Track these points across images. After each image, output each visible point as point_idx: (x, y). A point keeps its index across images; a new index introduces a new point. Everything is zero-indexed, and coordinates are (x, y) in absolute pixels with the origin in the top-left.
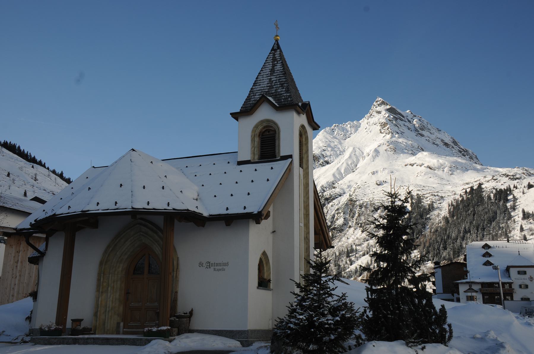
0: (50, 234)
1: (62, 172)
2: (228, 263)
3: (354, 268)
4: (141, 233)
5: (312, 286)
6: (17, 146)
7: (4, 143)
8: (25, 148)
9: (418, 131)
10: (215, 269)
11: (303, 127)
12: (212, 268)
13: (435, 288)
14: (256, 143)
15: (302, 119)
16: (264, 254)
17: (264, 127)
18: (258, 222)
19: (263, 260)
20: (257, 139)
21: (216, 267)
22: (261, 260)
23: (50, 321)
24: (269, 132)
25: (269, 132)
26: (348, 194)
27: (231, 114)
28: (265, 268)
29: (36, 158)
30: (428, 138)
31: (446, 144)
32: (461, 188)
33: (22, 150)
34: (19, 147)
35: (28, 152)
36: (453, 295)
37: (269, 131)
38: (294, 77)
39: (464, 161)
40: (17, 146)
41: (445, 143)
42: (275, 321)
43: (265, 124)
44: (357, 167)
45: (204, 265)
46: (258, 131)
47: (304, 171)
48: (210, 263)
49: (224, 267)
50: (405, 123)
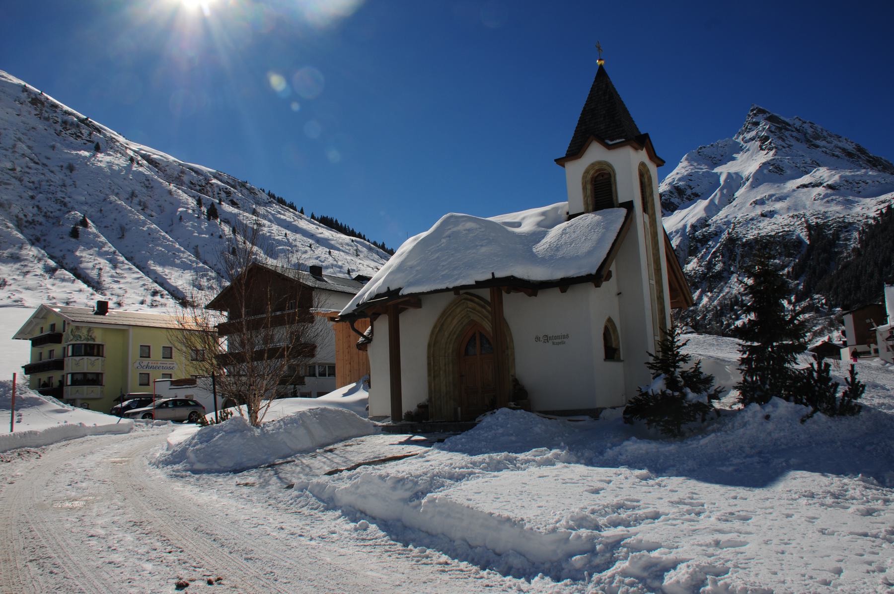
0: (374, 317)
2: (567, 335)
3: (741, 324)
4: (468, 309)
6: (334, 220)
7: (321, 218)
8: (342, 221)
9: (811, 141)
10: (553, 343)
11: (643, 164)
12: (550, 342)
13: (845, 340)
14: (589, 192)
15: (642, 156)
16: (610, 320)
17: (597, 171)
18: (598, 285)
19: (610, 327)
20: (589, 187)
21: (554, 341)
22: (606, 329)
24: (603, 176)
25: (603, 176)
26: (726, 232)
27: (556, 160)
28: (613, 337)
29: (355, 230)
30: (824, 149)
31: (849, 154)
32: (875, 209)
34: (336, 221)
36: (869, 346)
37: (602, 175)
38: (627, 106)
39: (875, 174)
40: (334, 220)
41: (848, 152)
43: (596, 168)
44: (735, 197)
45: (541, 339)
46: (589, 177)
47: (649, 218)
48: (547, 336)
49: (564, 340)
50: (792, 133)
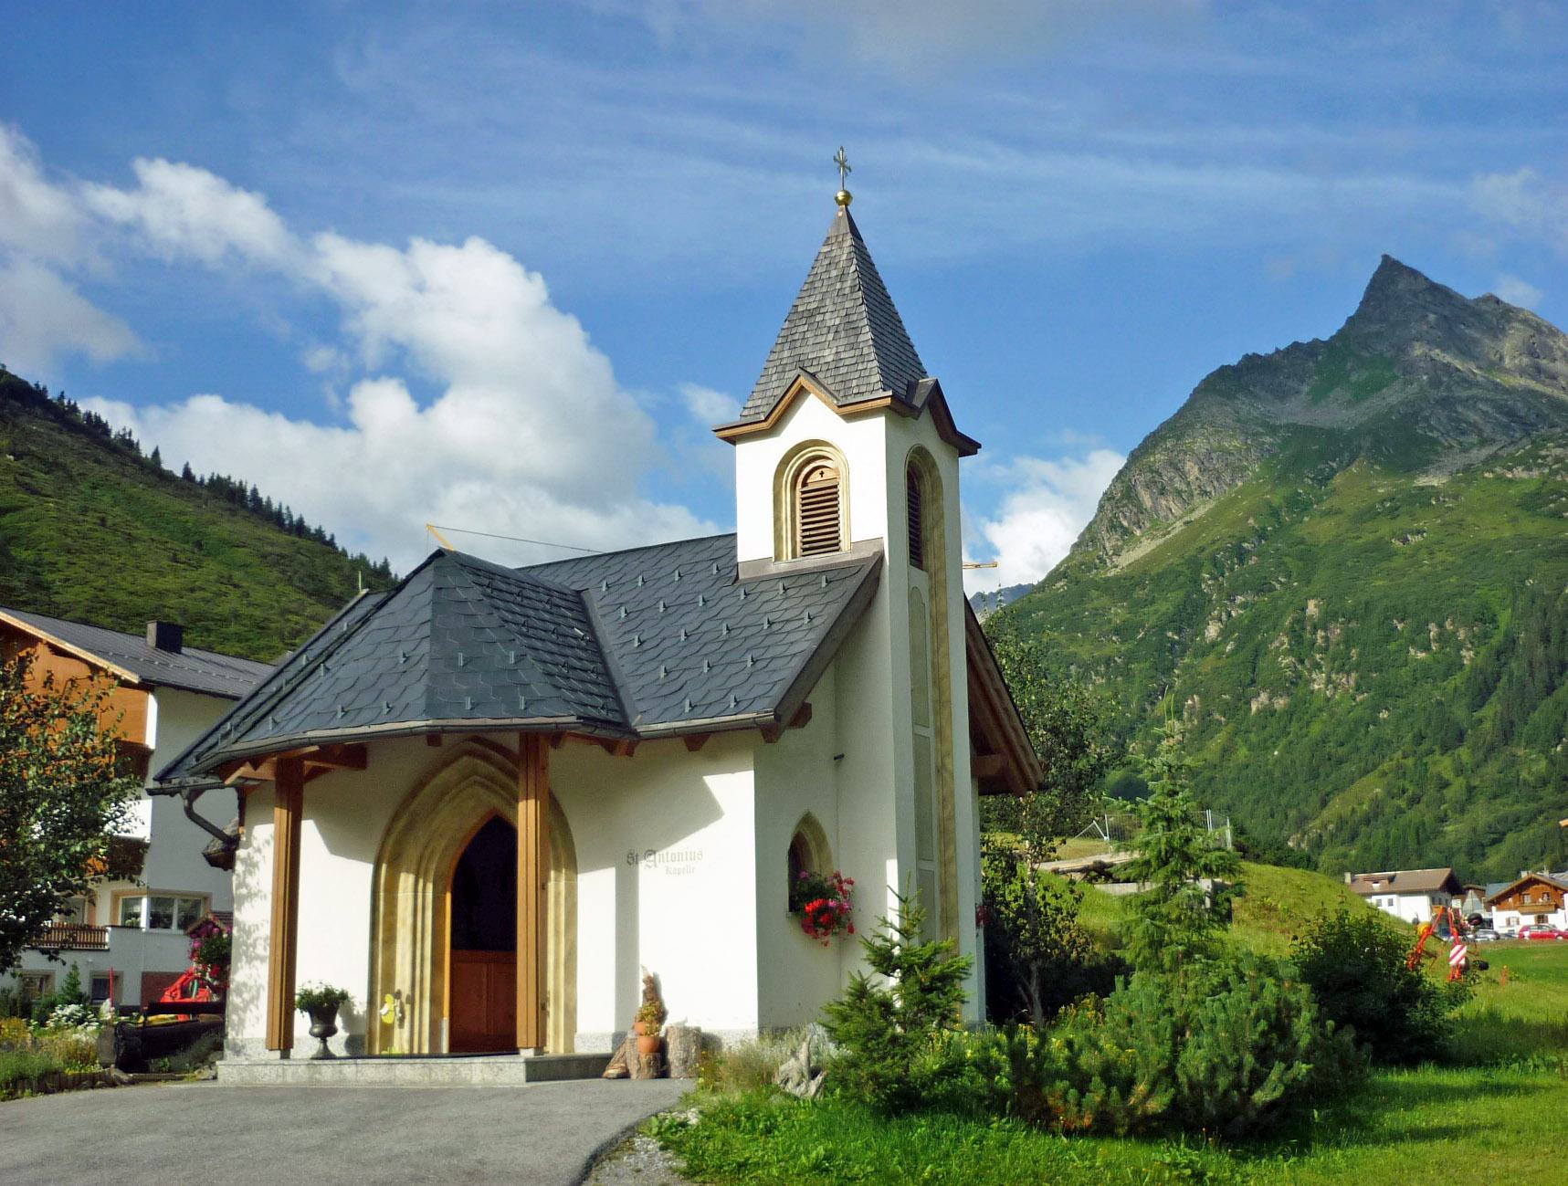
1: (386, 560)
5: (1503, 467)
23: (1484, 967)
33: (264, 500)
34: (255, 491)
35: (280, 506)
42: (1536, 941)
